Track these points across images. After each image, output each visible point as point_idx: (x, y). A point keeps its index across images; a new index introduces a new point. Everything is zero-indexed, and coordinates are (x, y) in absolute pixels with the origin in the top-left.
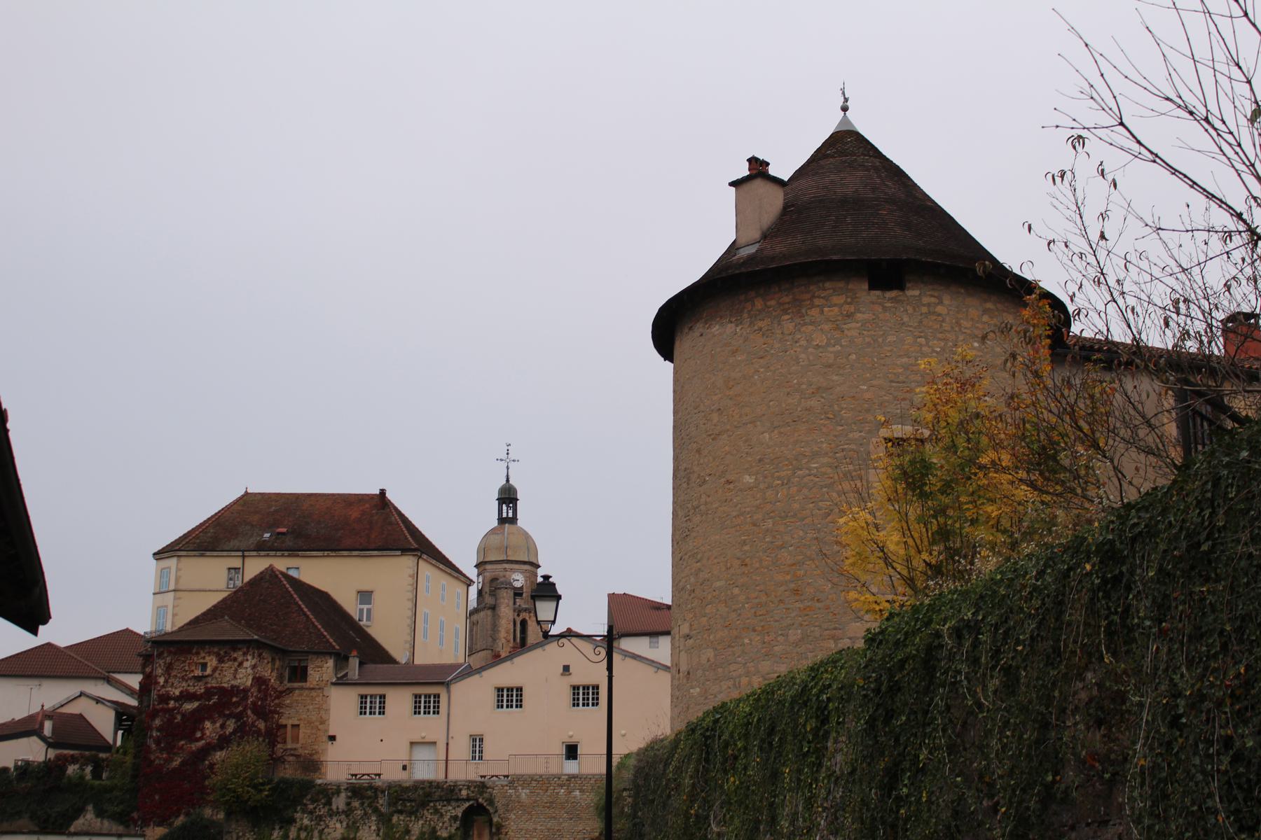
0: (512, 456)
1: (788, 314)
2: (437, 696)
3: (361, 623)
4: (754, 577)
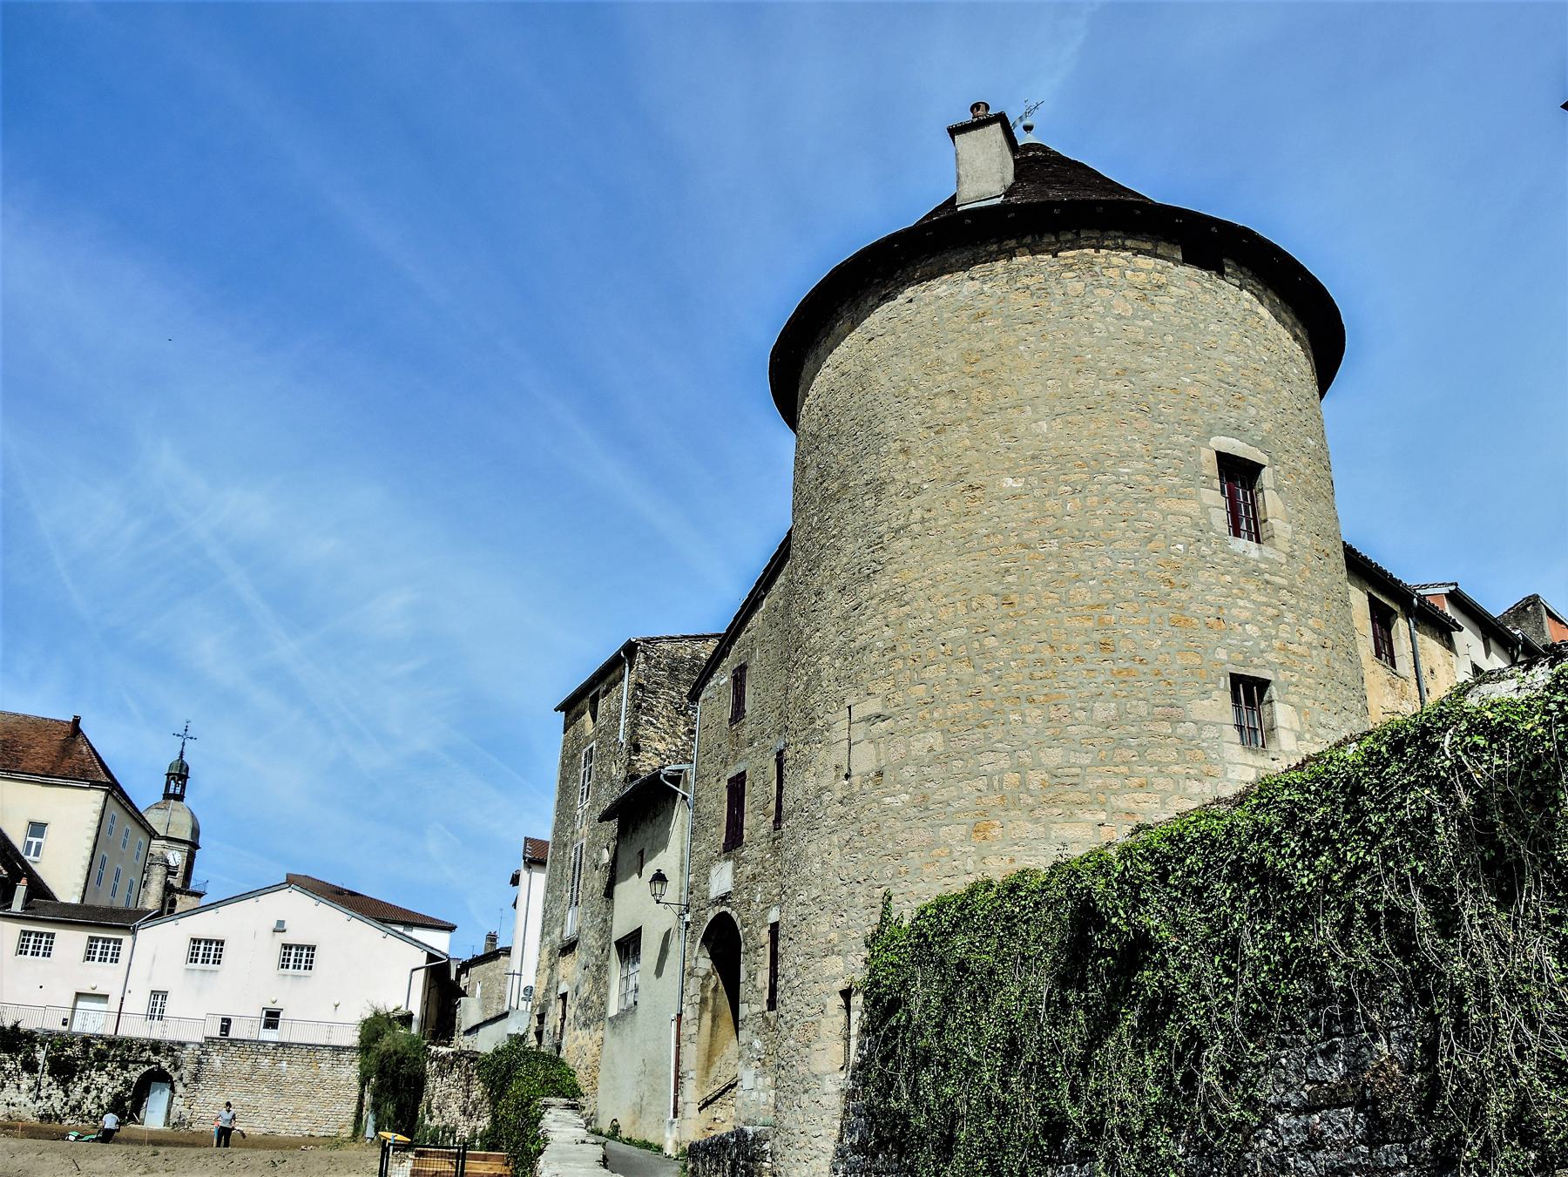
0: (190, 734)
1: (1073, 271)
2: (120, 941)
3: (27, 858)
4: (1028, 622)
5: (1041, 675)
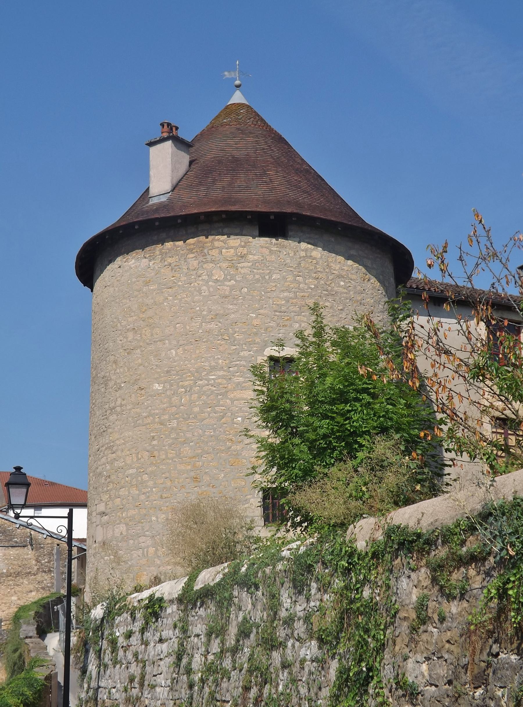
1: (193, 253)
5: (166, 496)
